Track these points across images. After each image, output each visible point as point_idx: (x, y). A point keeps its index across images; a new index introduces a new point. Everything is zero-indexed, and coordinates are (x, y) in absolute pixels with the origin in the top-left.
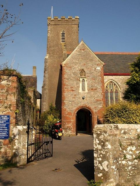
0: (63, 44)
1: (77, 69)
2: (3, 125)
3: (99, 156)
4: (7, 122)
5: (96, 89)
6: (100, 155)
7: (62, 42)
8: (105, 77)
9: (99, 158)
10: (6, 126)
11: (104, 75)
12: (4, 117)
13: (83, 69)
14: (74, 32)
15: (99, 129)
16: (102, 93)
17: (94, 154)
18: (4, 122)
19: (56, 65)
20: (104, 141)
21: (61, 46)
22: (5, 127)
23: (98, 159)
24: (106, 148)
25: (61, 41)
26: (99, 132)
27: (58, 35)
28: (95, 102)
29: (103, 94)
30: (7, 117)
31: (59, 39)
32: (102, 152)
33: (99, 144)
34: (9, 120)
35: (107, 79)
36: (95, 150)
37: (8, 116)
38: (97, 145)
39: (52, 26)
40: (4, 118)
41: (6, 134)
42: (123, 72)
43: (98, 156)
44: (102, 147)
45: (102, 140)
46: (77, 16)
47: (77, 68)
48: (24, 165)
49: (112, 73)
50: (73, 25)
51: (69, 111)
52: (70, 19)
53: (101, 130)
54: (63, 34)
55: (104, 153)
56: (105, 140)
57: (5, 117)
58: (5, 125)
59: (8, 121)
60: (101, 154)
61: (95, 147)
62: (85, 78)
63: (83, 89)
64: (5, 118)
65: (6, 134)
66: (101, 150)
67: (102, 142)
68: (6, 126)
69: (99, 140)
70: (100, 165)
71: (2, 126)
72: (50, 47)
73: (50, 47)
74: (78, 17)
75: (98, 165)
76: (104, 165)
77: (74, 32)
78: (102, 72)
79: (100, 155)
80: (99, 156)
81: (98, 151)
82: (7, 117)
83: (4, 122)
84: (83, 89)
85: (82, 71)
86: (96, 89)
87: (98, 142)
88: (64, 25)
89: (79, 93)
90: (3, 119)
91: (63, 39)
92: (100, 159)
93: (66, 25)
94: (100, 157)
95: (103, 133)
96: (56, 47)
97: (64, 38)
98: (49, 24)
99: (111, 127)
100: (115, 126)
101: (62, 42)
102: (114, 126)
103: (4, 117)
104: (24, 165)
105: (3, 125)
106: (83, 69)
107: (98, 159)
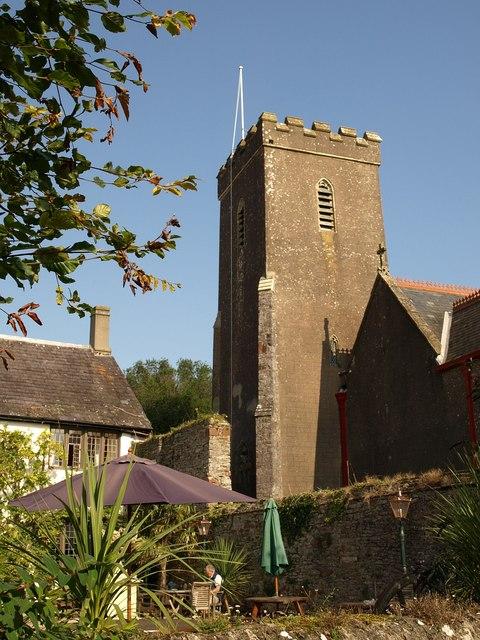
7: (322, 226)
14: (367, 196)
17: (210, 364)
19: (305, 324)
21: (323, 246)
25: (318, 196)
27: (305, 194)
46: (375, 131)
48: (466, 309)
50: (360, 166)
52: (350, 140)
54: (325, 197)
62: (472, 619)
74: (379, 138)
88: (327, 160)
91: (327, 214)
97: (325, 197)
98: (271, 141)
101: (322, 226)
104: (466, 309)
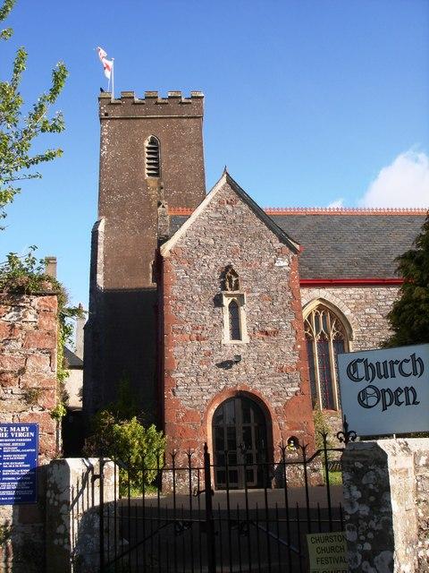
0: (152, 182)
1: (212, 267)
2: (16, 457)
3: (362, 538)
4: (28, 445)
5: (275, 333)
6: (365, 534)
8: (304, 291)
9: (362, 542)
10: (26, 461)
11: (303, 285)
12: (18, 429)
13: (229, 267)
14: (190, 144)
15: (358, 455)
16: (297, 344)
18: (19, 448)
20: (377, 491)
22: (21, 464)
23: (359, 547)
24: (385, 512)
26: (359, 465)
27: (136, 149)
28: (273, 375)
29: (299, 346)
30: (30, 431)
31: (139, 166)
32: (372, 524)
33: (360, 501)
34: (35, 439)
35: (311, 299)
36: (350, 521)
37: (33, 428)
38: (357, 504)
39: (116, 122)
40: (20, 435)
41: (27, 485)
42: (357, 273)
43: (358, 538)
44: (371, 508)
45: (371, 487)
47: (211, 265)
49: (323, 276)
50: (185, 120)
51: (187, 408)
53: (364, 456)
54: (155, 148)
55: (380, 527)
56: (380, 486)
57: (23, 429)
58: (23, 457)
59: (33, 443)
60: (371, 530)
61: (350, 512)
63: (236, 334)
64: (23, 434)
65: (27, 485)
66: (367, 519)
67: (372, 493)
68: (26, 461)
69: (362, 488)
70: (366, 563)
71: (14, 461)
72: (109, 192)
73: (109, 192)
75: (360, 566)
76: (380, 562)
77: (190, 144)
78: (294, 275)
79: (365, 534)
80: (362, 538)
81: (360, 522)
82: (30, 431)
83: (19, 448)
84: (236, 334)
85: (228, 276)
86: (275, 333)
87: (359, 494)
89: (221, 346)
90: (14, 438)
91: (156, 172)
92: (368, 547)
93: (162, 121)
94: (367, 540)
95: (372, 467)
96: (129, 193)
98: (106, 114)
99: (394, 448)
100: (402, 445)
102: (400, 444)
103: (18, 429)
105: (16, 457)
106: (229, 267)
107: (359, 547)
